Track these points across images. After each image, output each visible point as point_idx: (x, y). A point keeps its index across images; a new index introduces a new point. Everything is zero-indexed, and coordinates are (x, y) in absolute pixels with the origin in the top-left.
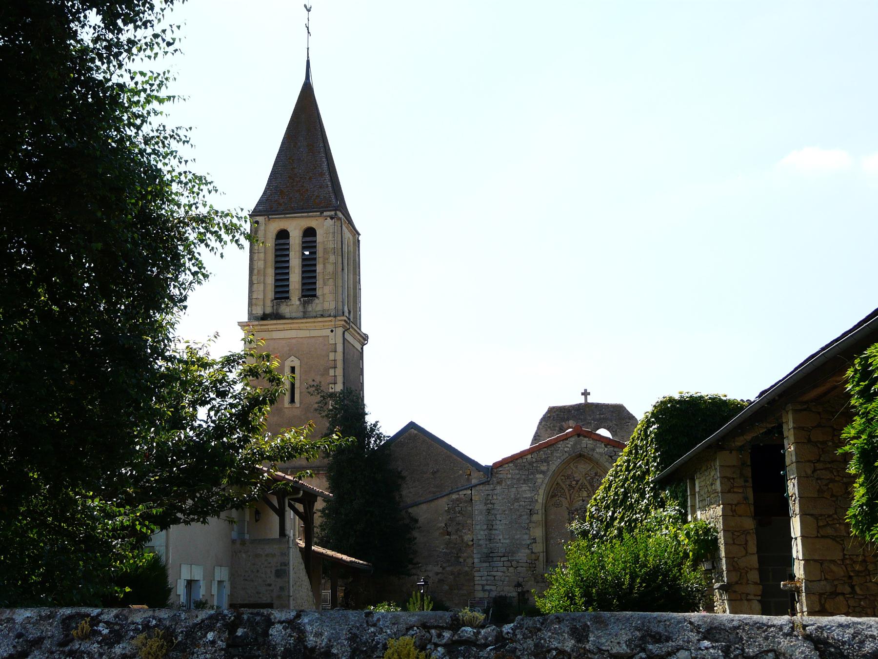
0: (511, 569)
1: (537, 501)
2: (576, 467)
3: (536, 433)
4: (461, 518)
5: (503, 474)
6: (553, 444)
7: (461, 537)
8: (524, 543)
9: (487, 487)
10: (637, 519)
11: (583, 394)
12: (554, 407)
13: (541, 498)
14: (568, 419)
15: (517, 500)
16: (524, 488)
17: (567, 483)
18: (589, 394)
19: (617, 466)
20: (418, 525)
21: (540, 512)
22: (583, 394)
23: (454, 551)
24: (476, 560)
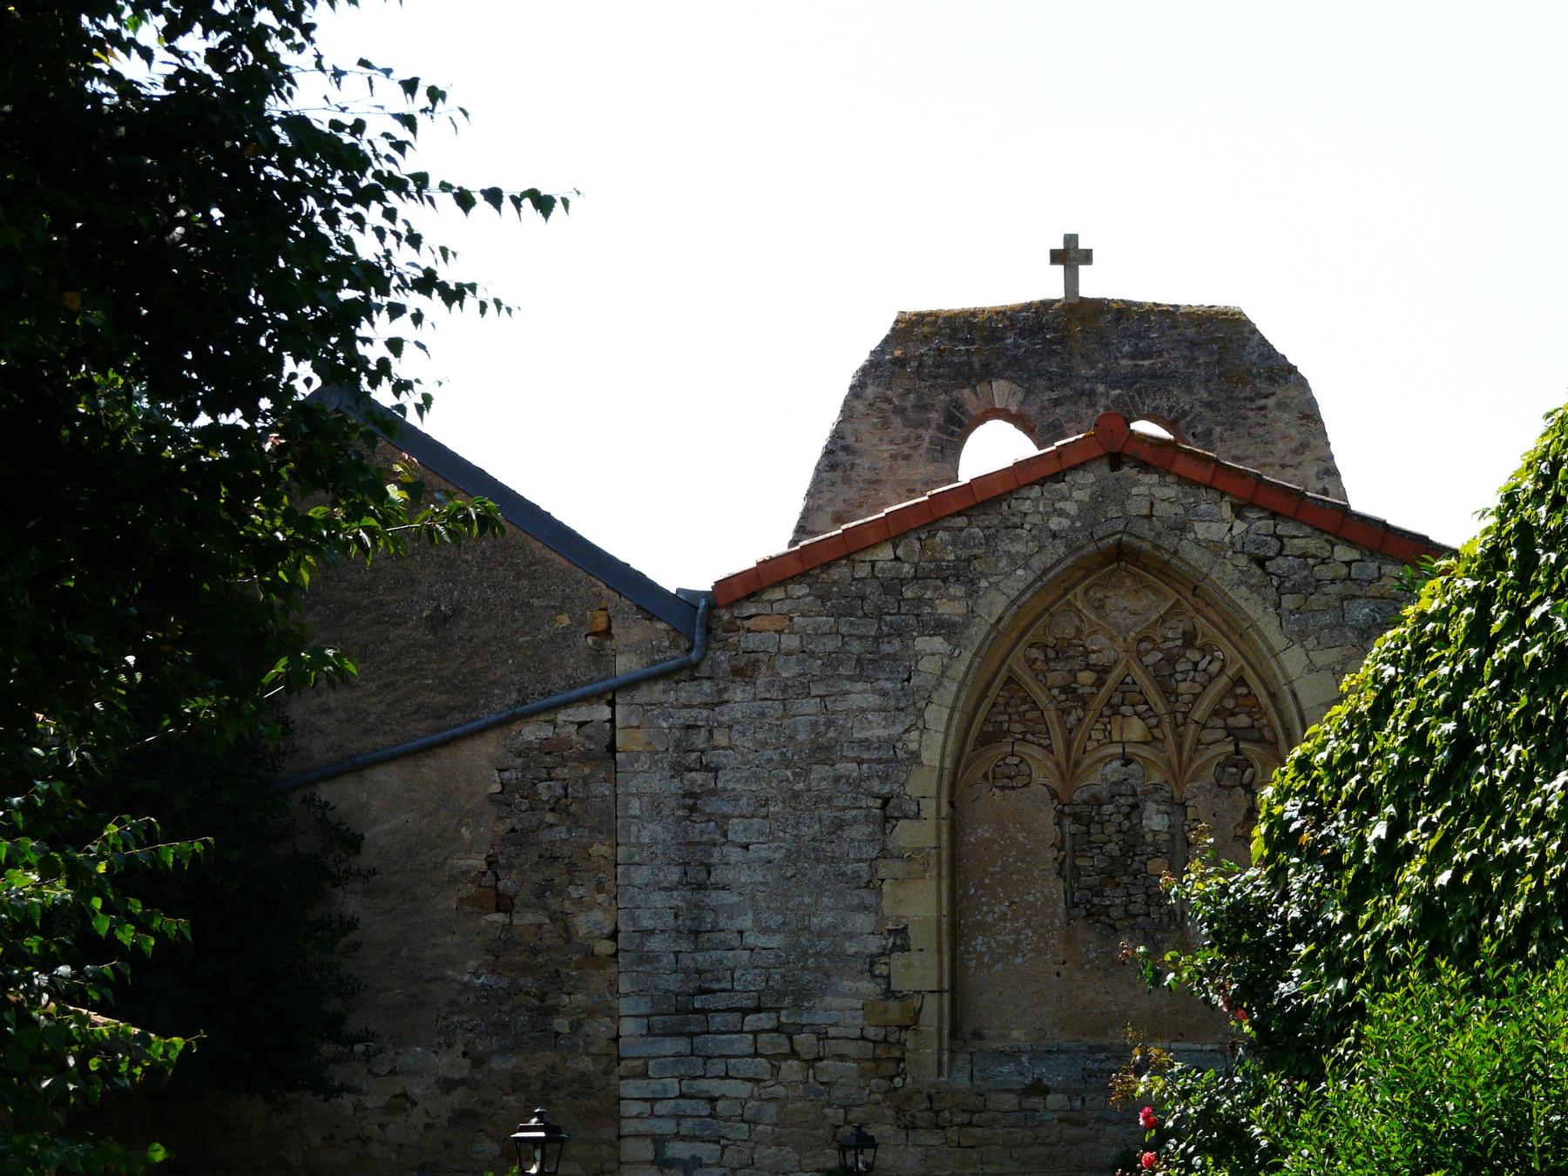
0: (791, 1068)
1: (915, 757)
2: (1100, 608)
3: (837, 435)
4: (561, 833)
5: (762, 630)
6: (998, 499)
7: (562, 921)
8: (851, 948)
9: (686, 691)
10: (1517, 857)
11: (1056, 257)
12: (920, 318)
13: (933, 745)
14: (988, 374)
15: (822, 752)
16: (855, 701)
17: (1057, 677)
18: (1087, 257)
19: (1423, 617)
20: (363, 862)
21: (929, 808)
22: (1056, 257)
23: (528, 983)
24: (628, 1027)
